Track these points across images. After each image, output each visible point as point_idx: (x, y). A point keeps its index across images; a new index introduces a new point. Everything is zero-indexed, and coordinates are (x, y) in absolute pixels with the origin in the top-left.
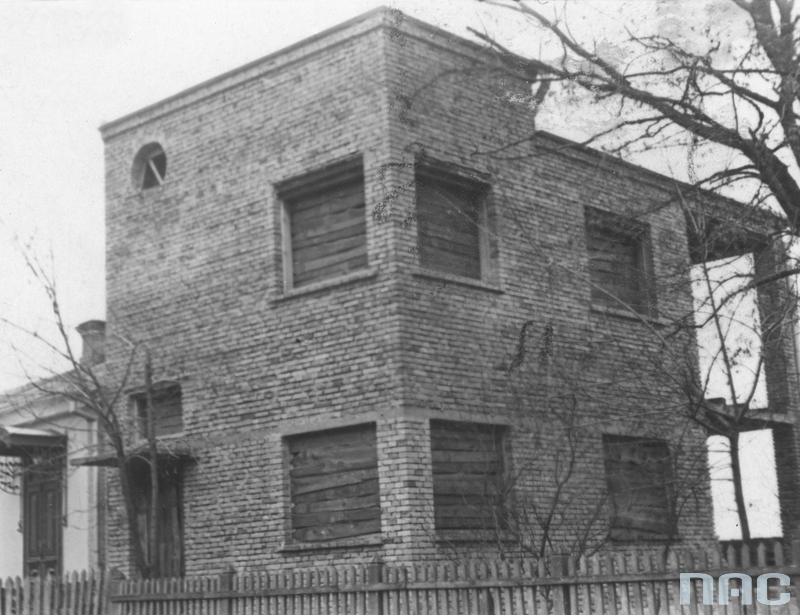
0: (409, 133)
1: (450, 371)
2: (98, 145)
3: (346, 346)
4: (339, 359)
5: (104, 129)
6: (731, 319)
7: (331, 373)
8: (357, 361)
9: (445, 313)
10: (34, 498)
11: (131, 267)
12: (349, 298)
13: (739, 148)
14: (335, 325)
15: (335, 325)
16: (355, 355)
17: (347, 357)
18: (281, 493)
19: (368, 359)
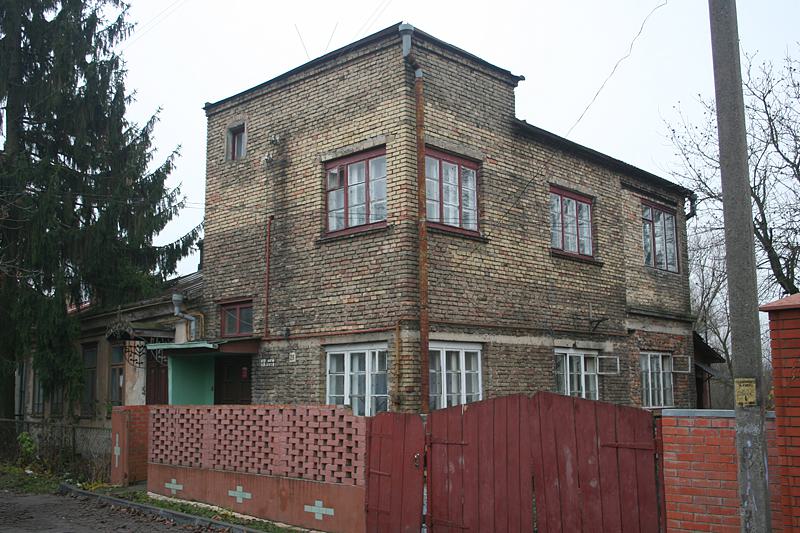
0: (120, 68)
1: (444, 303)
2: (202, 119)
3: (369, 281)
4: (362, 290)
5: (209, 108)
6: (786, 446)
7: (357, 300)
8: (376, 293)
9: (442, 259)
10: (153, 371)
11: (219, 215)
12: (372, 245)
13: (560, 149)
14: (361, 264)
15: (361, 264)
16: (375, 289)
17: (369, 289)
18: (318, 387)
19: (384, 292)
